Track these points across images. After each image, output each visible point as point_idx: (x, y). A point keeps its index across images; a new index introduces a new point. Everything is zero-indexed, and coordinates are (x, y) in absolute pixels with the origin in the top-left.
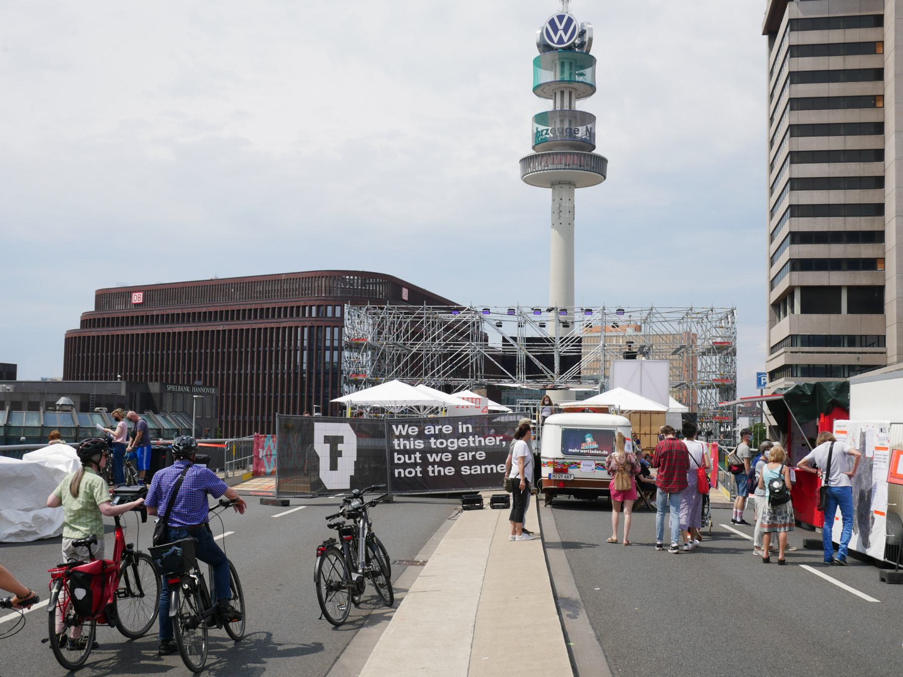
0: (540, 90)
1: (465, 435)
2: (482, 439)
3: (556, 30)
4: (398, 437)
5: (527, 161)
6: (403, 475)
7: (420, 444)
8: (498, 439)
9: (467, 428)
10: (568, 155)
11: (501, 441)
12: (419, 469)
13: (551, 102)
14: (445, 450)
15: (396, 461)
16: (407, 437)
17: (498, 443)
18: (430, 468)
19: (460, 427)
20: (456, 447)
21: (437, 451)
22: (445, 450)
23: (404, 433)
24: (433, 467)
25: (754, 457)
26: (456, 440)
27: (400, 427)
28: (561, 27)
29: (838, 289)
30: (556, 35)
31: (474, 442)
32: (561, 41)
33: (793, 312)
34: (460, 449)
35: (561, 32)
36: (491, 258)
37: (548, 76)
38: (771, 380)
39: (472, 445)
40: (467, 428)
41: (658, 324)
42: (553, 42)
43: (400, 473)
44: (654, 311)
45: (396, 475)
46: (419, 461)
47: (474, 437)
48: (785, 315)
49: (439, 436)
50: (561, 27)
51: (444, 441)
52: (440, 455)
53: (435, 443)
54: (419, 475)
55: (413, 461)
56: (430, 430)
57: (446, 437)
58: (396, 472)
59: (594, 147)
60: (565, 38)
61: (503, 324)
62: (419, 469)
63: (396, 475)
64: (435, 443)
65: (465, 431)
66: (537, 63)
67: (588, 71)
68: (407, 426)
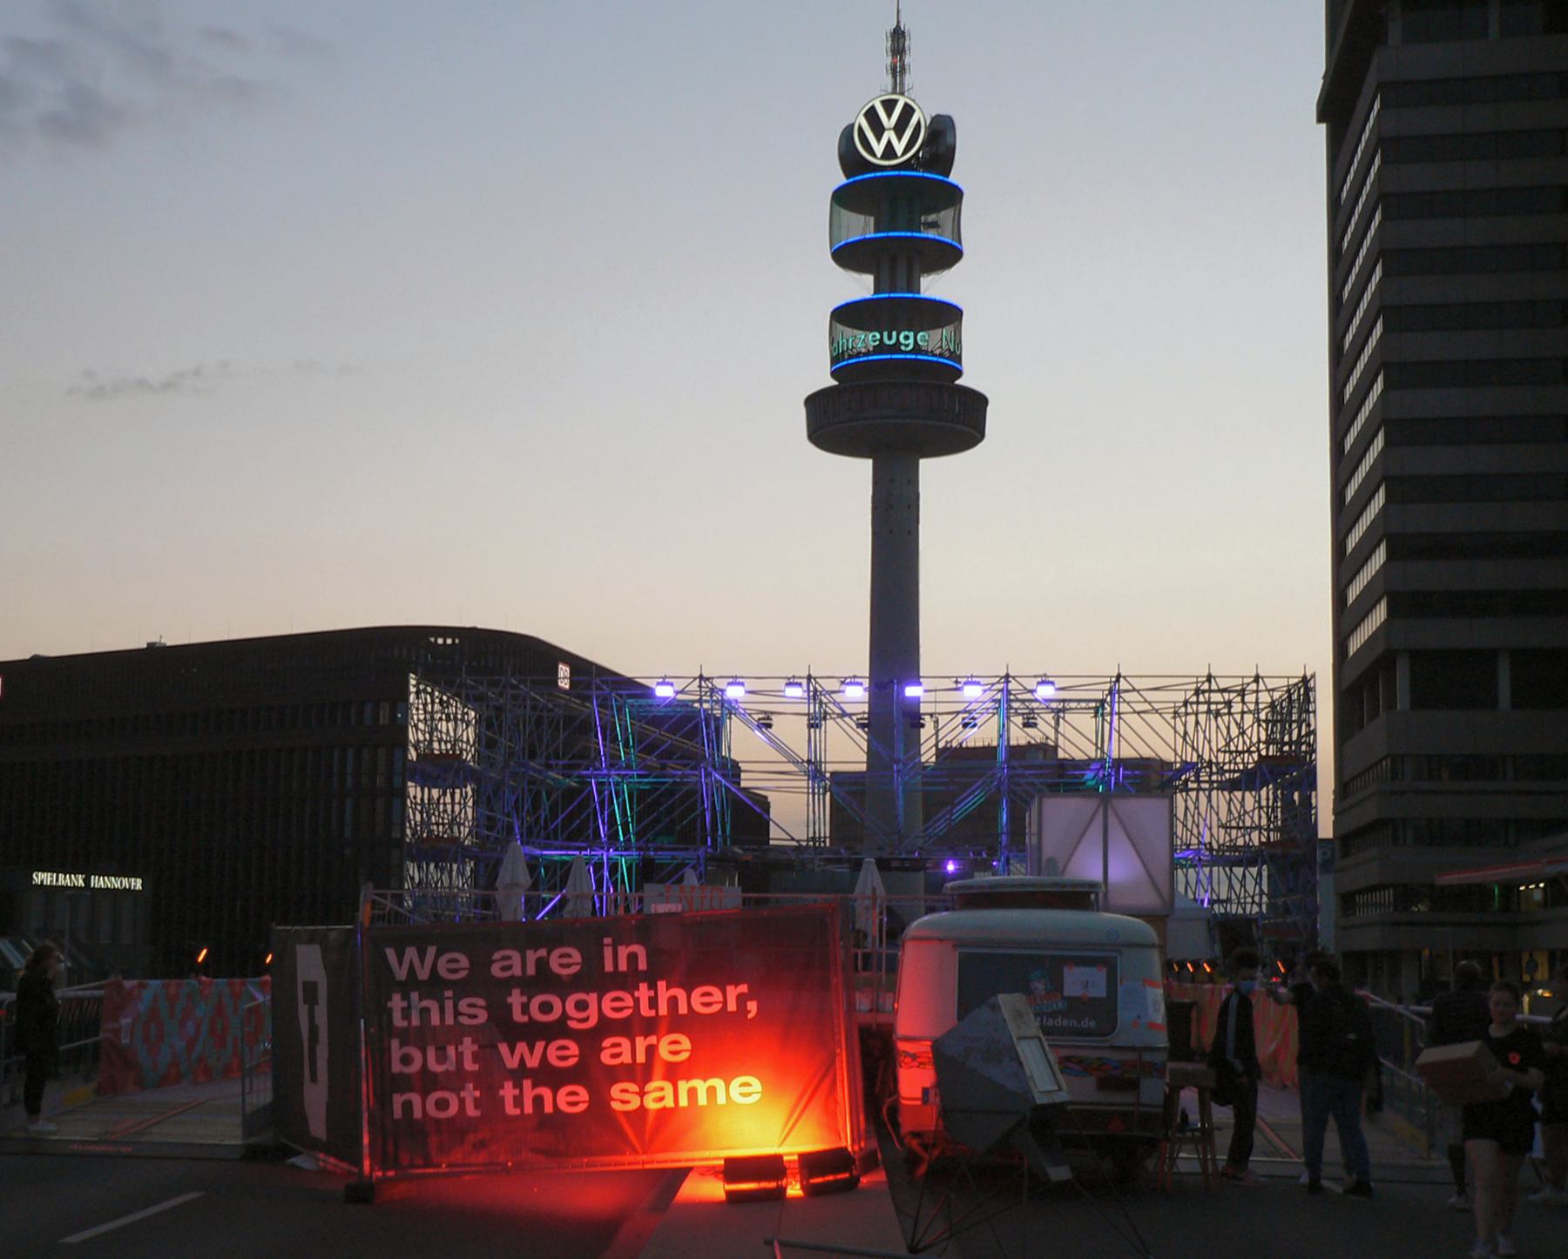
0: (848, 256)
1: (627, 981)
2: (680, 994)
3: (879, 130)
4: (405, 988)
5: (817, 404)
6: (418, 1114)
7: (475, 1011)
8: (732, 992)
9: (632, 958)
10: (897, 406)
11: (742, 1000)
12: (470, 1093)
13: (869, 279)
14: (560, 1029)
15: (397, 1067)
16: (434, 986)
17: (732, 1007)
18: (508, 1092)
19: (608, 952)
20: (593, 1021)
21: (534, 1033)
22: (560, 1029)
23: (423, 974)
24: (518, 1085)
25: (1487, 1039)
26: (592, 999)
27: (411, 953)
28: (889, 122)
29: (1494, 653)
30: (879, 139)
31: (653, 1003)
32: (889, 152)
33: (1391, 705)
34: (606, 1027)
35: (889, 135)
36: (712, 580)
37: (860, 227)
38: (1346, 855)
39: (645, 1011)
40: (632, 958)
41: (1133, 719)
42: (874, 155)
43: (408, 1106)
44: (1123, 685)
45: (398, 1112)
46: (470, 1066)
47: (653, 986)
48: (1375, 714)
49: (544, 980)
50: (889, 122)
51: (556, 1002)
52: (540, 1045)
53: (525, 1009)
54: (471, 1111)
55: (450, 1066)
56: (510, 962)
57: (563, 987)
58: (398, 1100)
59: (959, 373)
60: (899, 147)
61: (775, 719)
62: (470, 1093)
63: (398, 1112)
64: (525, 1009)
65: (623, 967)
66: (841, 198)
67: (945, 216)
68: (431, 951)
